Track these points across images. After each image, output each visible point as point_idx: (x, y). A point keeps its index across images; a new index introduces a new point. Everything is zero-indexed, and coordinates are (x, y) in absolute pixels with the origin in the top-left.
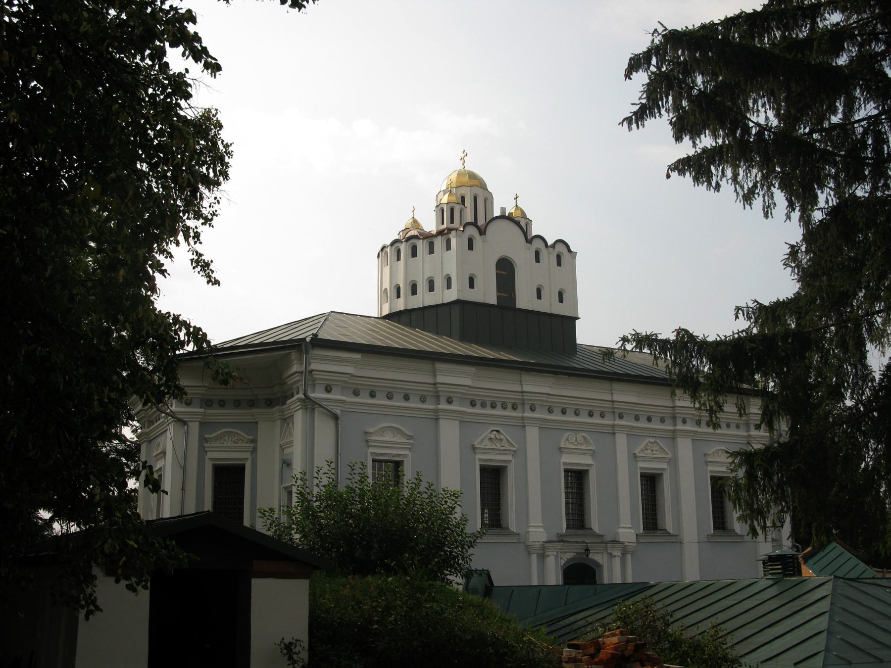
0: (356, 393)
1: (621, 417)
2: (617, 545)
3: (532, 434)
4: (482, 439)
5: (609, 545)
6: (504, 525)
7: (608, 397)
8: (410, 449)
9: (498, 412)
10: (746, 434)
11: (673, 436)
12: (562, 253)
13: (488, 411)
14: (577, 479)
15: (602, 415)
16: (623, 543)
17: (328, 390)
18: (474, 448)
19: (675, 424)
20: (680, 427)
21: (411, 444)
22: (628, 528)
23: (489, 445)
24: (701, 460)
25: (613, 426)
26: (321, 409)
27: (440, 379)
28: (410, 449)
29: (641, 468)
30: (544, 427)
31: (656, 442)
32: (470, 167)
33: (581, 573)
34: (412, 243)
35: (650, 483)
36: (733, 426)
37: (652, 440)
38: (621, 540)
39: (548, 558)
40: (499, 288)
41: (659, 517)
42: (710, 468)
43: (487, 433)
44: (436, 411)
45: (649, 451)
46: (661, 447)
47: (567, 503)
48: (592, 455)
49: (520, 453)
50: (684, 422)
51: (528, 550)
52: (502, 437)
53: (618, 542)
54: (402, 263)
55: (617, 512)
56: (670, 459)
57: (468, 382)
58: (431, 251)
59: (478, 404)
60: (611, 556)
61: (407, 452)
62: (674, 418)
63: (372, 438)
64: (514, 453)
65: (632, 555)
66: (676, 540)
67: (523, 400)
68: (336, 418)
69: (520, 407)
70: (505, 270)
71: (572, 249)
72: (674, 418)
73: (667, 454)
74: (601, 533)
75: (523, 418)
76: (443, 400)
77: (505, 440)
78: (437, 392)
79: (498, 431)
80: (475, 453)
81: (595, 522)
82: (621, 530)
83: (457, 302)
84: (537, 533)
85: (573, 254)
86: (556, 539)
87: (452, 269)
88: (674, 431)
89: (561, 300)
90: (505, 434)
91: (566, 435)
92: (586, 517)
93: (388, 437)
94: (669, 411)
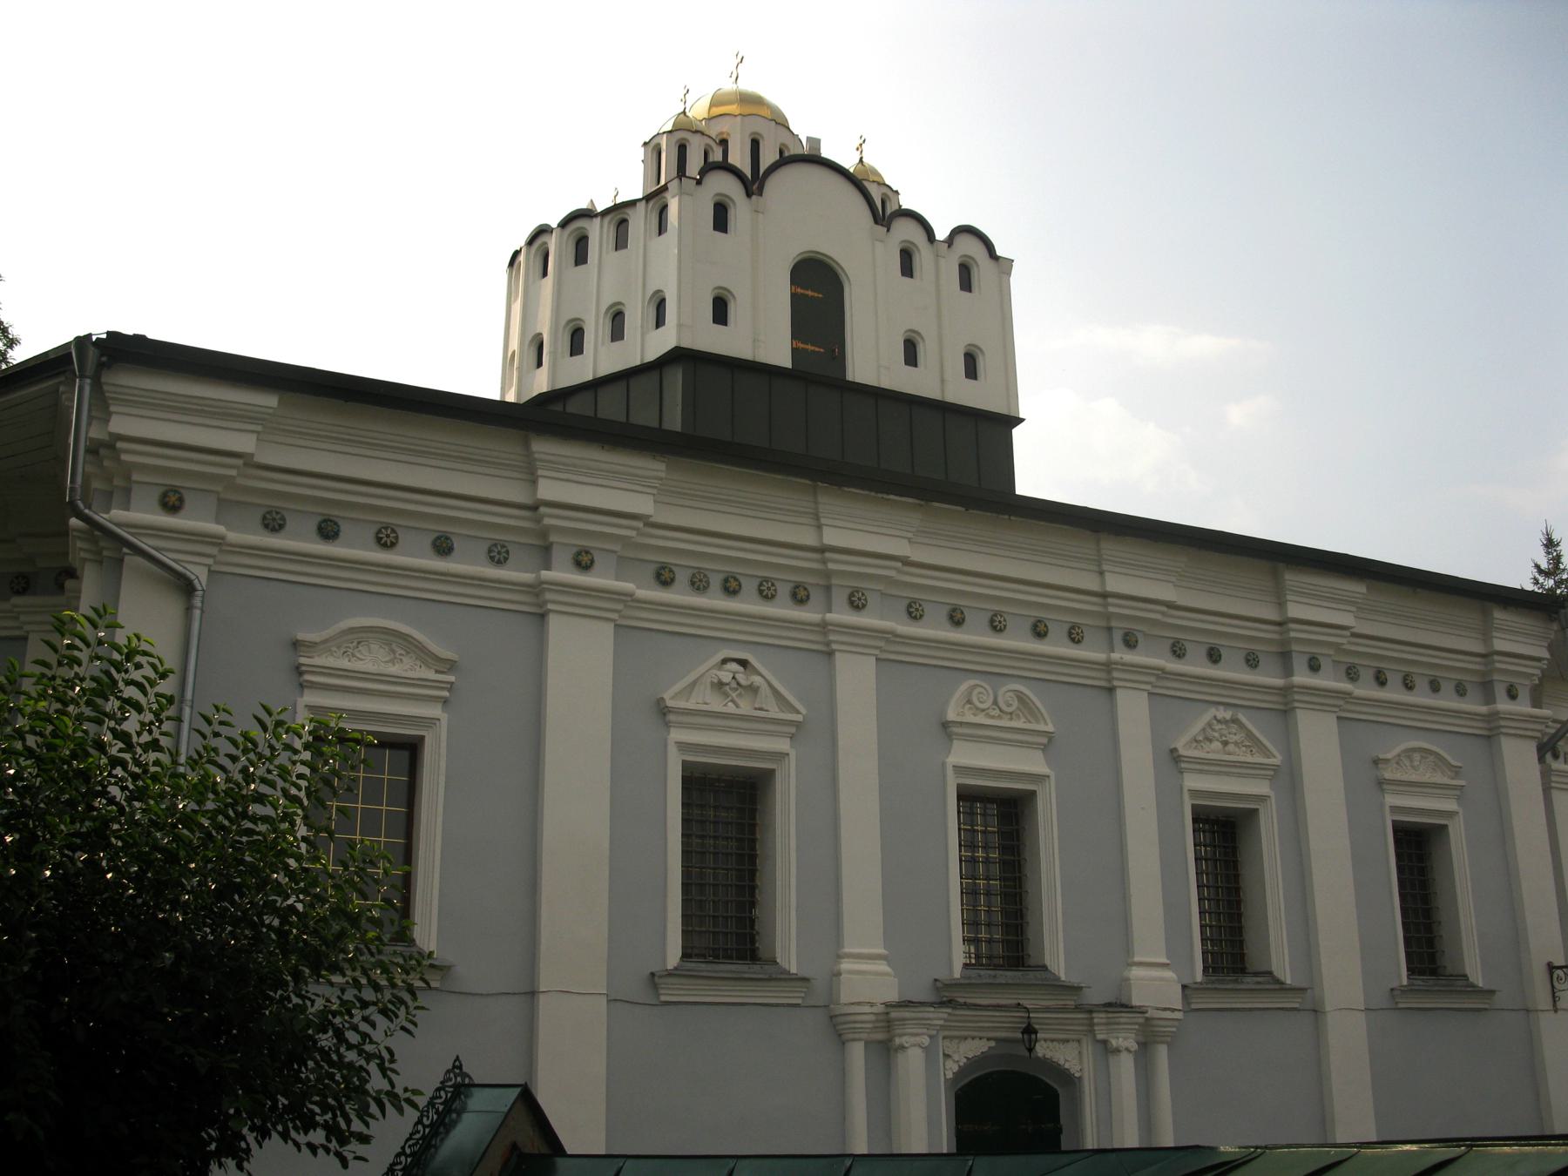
0: (274, 523)
1: (1130, 642)
2: (1124, 1017)
3: (856, 679)
4: (693, 683)
5: (1099, 1018)
6: (763, 952)
7: (1091, 583)
8: (445, 701)
9: (747, 604)
10: (1483, 709)
11: (1284, 706)
12: (975, 260)
13: (715, 600)
14: (999, 823)
15: (1075, 637)
16: (1141, 1011)
17: (171, 504)
18: (663, 711)
19: (1288, 671)
20: (1302, 678)
21: (451, 687)
22: (1157, 961)
23: (716, 704)
24: (1369, 777)
25: (1108, 666)
26: (139, 560)
27: (548, 490)
28: (445, 701)
29: (1194, 793)
30: (892, 656)
31: (1235, 721)
32: (748, 85)
33: (1011, 1108)
34: (576, 237)
35: (1223, 836)
36: (1448, 688)
37: (1223, 714)
38: (1135, 1002)
39: (900, 1057)
40: (799, 328)
41: (1250, 936)
42: (1391, 800)
43: (707, 666)
44: (536, 590)
45: (1217, 745)
46: (1250, 735)
47: (969, 893)
48: (1045, 749)
49: (818, 729)
50: (1314, 666)
51: (837, 1028)
52: (757, 680)
53: (1125, 1007)
54: (548, 283)
55: (1123, 918)
56: (1276, 769)
57: (642, 504)
58: (621, 242)
59: (682, 578)
60: (1107, 1049)
61: (434, 711)
62: (1285, 658)
63: (317, 661)
64: (796, 731)
65: (1169, 1044)
66: (1304, 1003)
67: (828, 574)
68: (185, 587)
69: (816, 597)
70: (817, 289)
71: (999, 253)
72: (1285, 658)
73: (1268, 754)
74: (1074, 980)
75: (824, 627)
76: (562, 556)
77: (764, 687)
78: (544, 533)
79: (743, 663)
80: (667, 725)
81: (1057, 946)
82: (1136, 972)
83: (678, 356)
84: (868, 977)
85: (1003, 266)
86: (931, 999)
87: (666, 279)
88: (1286, 691)
89: (971, 371)
90: (766, 672)
91: (964, 687)
92: (1030, 933)
93: (372, 660)
94: (1270, 633)
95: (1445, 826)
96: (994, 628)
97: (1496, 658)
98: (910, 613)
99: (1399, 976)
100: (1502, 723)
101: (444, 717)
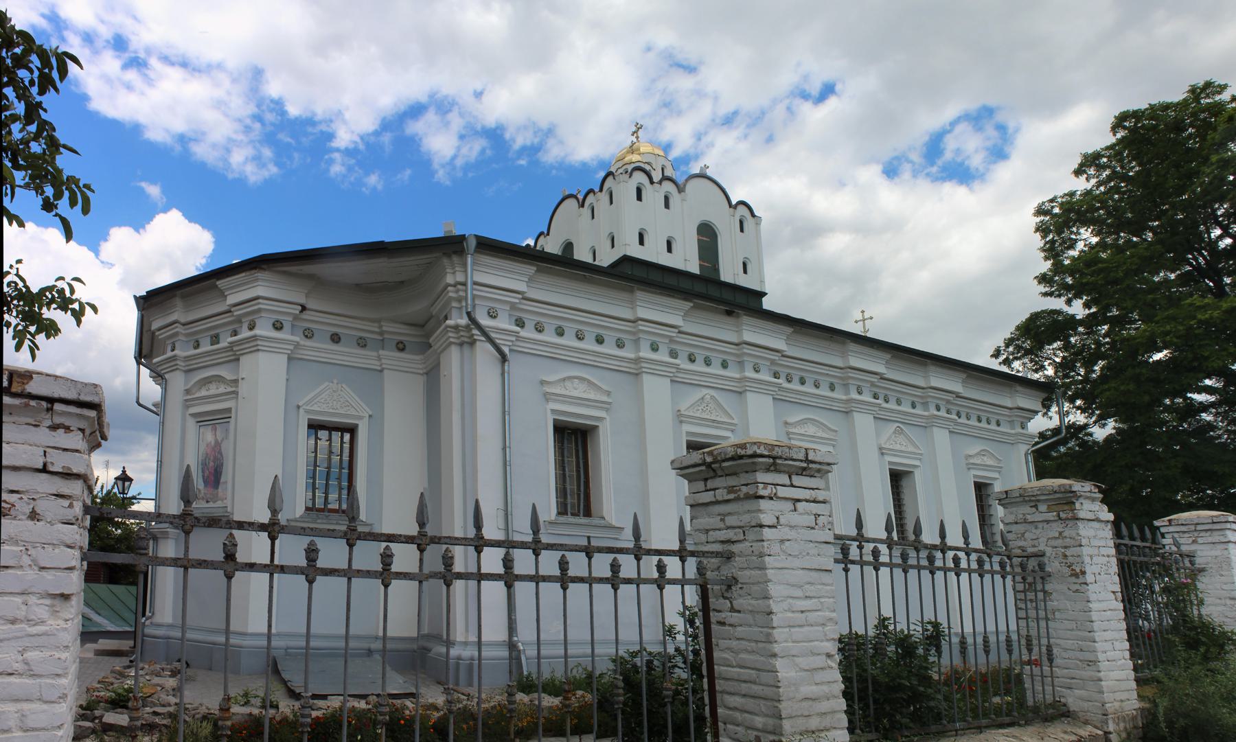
61: (996, 475)
62: (741, 364)
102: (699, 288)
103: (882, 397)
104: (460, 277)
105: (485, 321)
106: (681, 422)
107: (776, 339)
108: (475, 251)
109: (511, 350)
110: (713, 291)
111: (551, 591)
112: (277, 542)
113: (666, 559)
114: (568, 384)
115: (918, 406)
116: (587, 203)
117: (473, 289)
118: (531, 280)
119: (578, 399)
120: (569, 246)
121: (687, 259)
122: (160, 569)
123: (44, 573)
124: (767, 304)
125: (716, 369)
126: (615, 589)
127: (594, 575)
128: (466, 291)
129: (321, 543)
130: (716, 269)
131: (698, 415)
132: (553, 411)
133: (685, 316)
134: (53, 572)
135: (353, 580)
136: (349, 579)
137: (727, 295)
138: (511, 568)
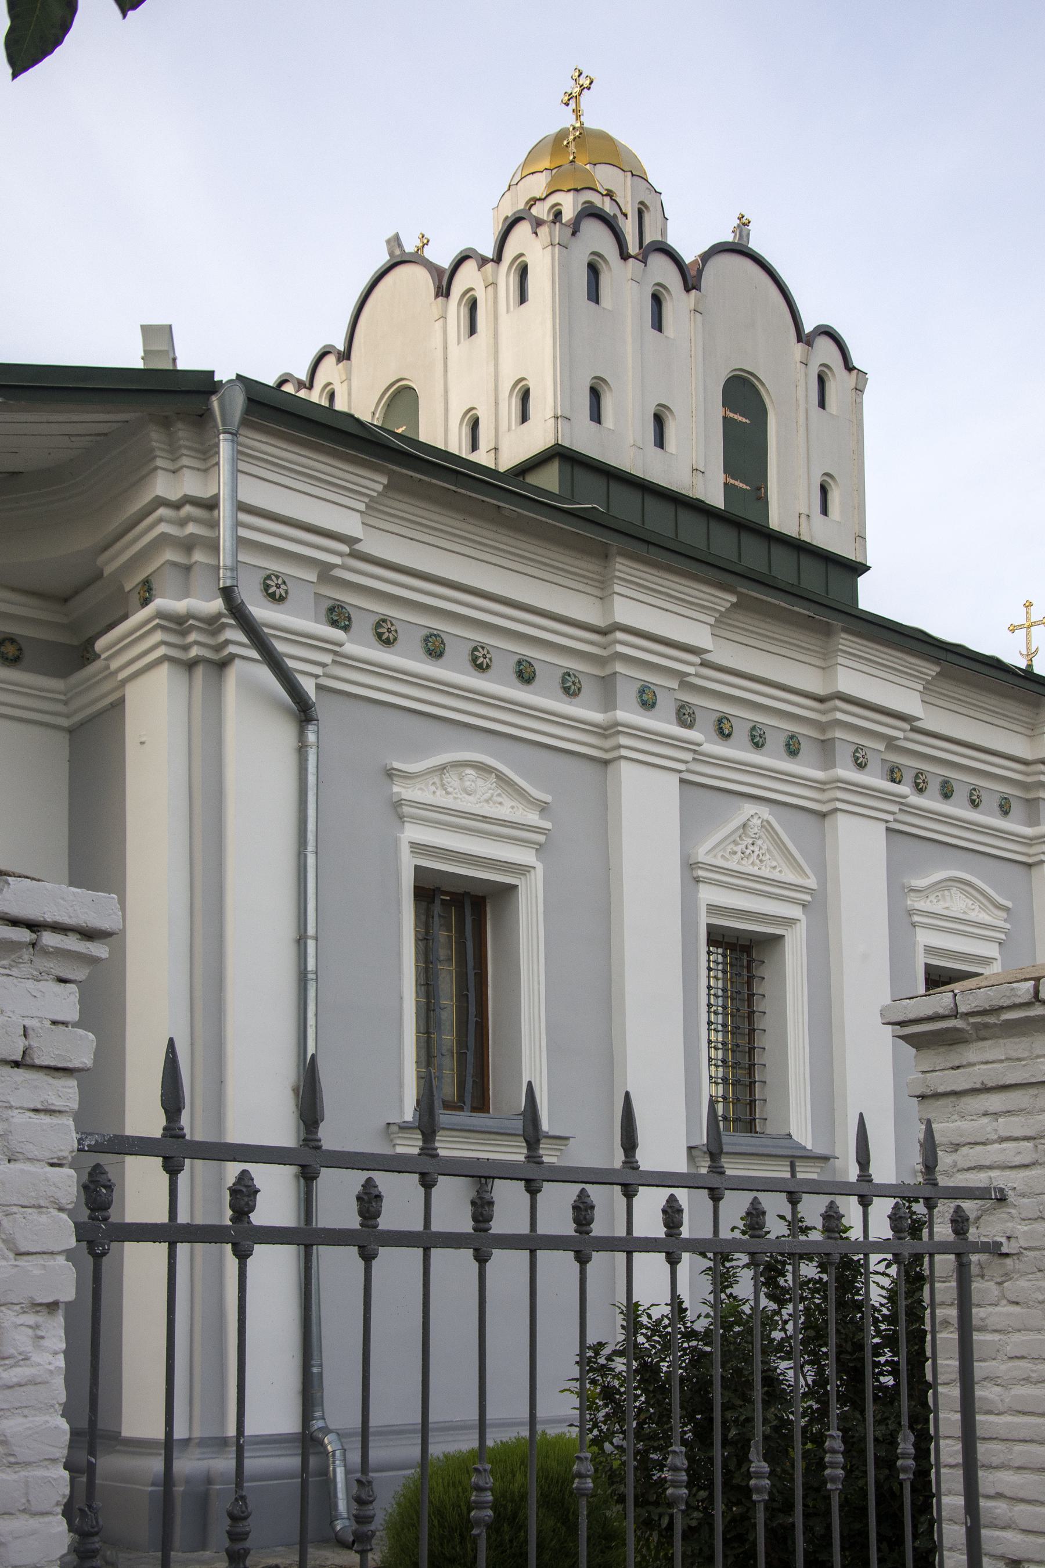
10: (598, 717)
26: (265, 675)
61: (796, 912)
62: (826, 749)
85: (859, 379)
95: (780, 938)
96: (566, 690)
97: (619, 635)
98: (379, 636)
99: (702, 1138)
100: (623, 740)
101: (539, 866)
102: (723, 543)
103: (908, 777)
104: (191, 485)
105: (261, 611)
106: (697, 880)
107: (897, 689)
108: (245, 422)
109: (319, 687)
110: (754, 555)
111: (454, 1266)
112: (183, 1178)
113: (384, 1181)
114: (452, 779)
115: (1016, 807)
116: (458, 288)
117: (238, 524)
118: (373, 508)
119: (462, 810)
120: (402, 397)
121: (693, 464)
122: (131, 1249)
123: (23, 1262)
124: (873, 596)
125: (542, 697)
126: (368, 1257)
127: (436, 1227)
128: (214, 525)
129: (384, 1181)
130: (760, 496)
131: (732, 865)
132: (417, 848)
133: (721, 623)
134: (40, 1260)
135: (434, 1251)
136: (533, 1253)
137: (783, 565)
138: (105, 1206)
